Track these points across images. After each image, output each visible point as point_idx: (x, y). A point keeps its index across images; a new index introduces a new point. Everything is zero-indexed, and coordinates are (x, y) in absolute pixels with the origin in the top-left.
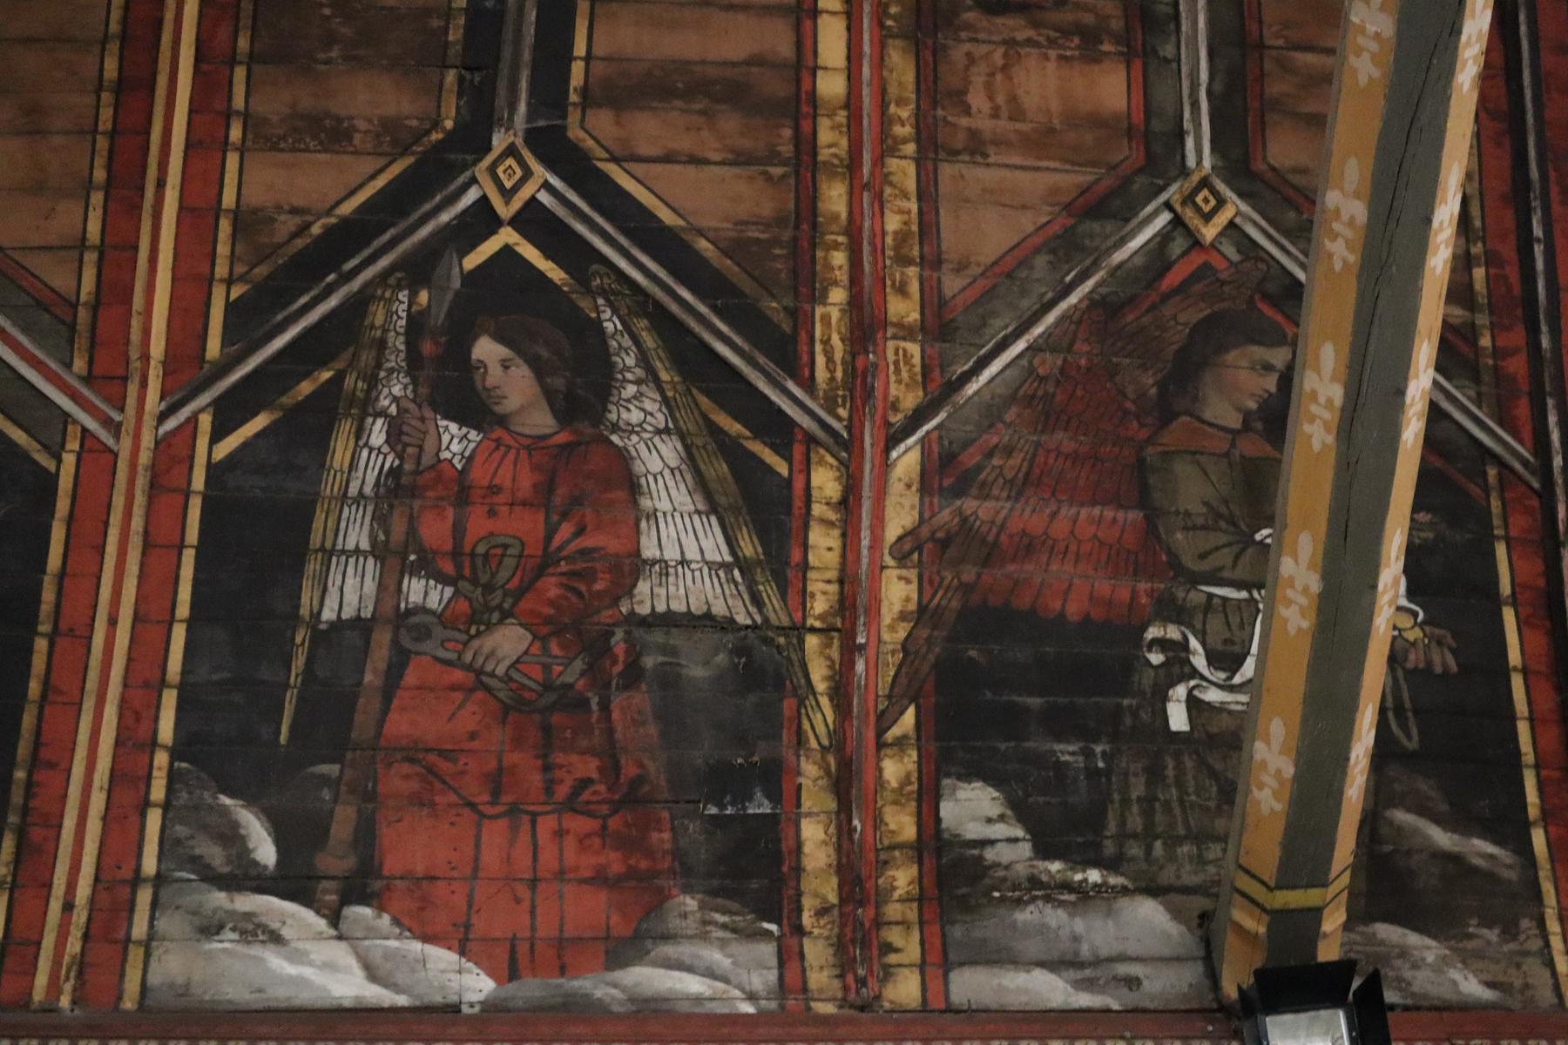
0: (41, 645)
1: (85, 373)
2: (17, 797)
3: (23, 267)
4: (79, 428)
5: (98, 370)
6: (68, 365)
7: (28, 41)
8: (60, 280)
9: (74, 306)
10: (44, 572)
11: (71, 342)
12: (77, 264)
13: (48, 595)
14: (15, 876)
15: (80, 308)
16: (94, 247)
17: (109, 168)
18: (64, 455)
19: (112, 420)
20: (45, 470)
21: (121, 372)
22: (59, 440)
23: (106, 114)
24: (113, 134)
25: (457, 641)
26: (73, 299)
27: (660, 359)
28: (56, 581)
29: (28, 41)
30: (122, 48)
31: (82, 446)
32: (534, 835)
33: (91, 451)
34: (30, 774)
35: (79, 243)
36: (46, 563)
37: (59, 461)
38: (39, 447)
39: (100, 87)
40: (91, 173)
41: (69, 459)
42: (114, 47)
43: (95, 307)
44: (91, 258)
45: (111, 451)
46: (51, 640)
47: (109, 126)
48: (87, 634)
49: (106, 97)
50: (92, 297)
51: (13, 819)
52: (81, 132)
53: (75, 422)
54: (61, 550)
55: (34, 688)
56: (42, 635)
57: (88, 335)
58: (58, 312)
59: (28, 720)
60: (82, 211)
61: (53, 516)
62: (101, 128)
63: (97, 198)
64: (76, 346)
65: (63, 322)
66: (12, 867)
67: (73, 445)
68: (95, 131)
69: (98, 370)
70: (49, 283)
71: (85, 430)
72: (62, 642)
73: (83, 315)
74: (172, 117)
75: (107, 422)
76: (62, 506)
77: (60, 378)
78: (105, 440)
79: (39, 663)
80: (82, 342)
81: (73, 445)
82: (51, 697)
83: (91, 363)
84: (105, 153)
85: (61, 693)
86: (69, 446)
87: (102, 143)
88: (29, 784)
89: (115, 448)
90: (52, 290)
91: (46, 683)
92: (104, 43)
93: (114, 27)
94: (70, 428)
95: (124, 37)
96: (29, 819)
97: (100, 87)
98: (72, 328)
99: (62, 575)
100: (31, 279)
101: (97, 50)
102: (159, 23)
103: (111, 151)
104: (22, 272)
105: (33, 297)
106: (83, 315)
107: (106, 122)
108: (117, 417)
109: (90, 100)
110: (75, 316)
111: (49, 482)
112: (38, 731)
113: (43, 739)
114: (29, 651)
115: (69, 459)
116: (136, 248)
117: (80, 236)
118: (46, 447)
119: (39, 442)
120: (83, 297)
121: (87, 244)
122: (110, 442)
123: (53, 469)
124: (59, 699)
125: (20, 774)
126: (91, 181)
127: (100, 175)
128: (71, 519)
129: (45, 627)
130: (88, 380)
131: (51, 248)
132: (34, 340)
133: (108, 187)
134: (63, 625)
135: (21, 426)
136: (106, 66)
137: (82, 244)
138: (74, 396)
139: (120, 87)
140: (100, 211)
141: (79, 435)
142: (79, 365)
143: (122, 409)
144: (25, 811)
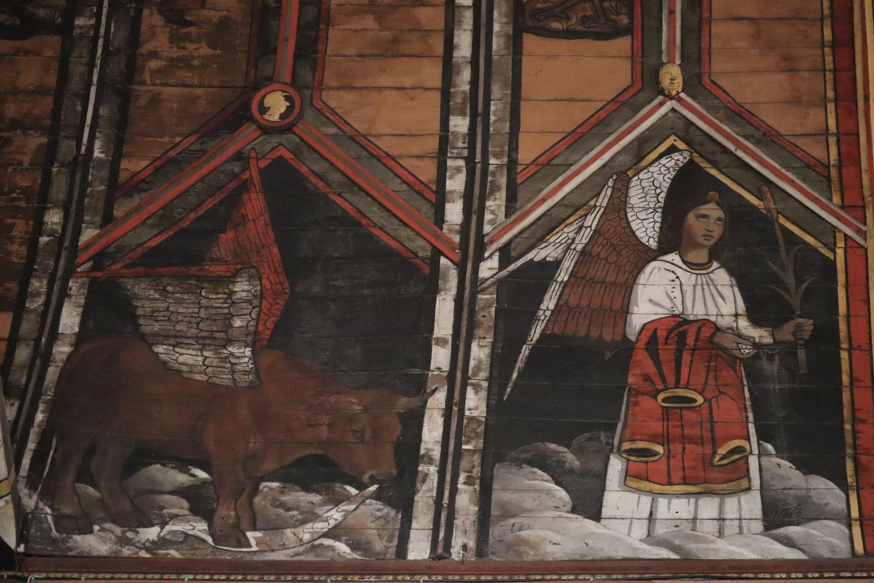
0: (844, 355)
1: (840, 204)
2: (849, 439)
3: (796, 146)
4: (843, 235)
5: (847, 202)
6: (831, 200)
7: (780, 19)
8: (817, 152)
9: (828, 167)
10: (838, 314)
11: (830, 187)
12: (825, 144)
13: (843, 327)
14: (857, 482)
15: (831, 168)
16: (833, 134)
17: (835, 89)
18: (837, 250)
19: (862, 230)
20: (828, 258)
21: (861, 204)
22: (833, 241)
23: (829, 59)
24: (835, 71)
25: (598, 239)
26: (827, 163)
27: (709, 85)
28: (845, 319)
29: (780, 19)
30: (832, 23)
31: (846, 244)
32: (148, 240)
33: (851, 247)
34: (853, 426)
35: (825, 132)
36: (838, 310)
37: (835, 253)
38: (822, 246)
39: (823, 45)
40: (826, 93)
41: (840, 252)
42: (828, 23)
43: (840, 167)
44: (832, 140)
45: (863, 247)
46: (850, 351)
47: (831, 66)
48: (869, 349)
49: (827, 50)
50: (837, 162)
51: (849, 451)
52: (818, 70)
53: (840, 231)
54: (845, 302)
55: (845, 379)
56: (844, 349)
57: (839, 183)
58: (818, 170)
59: (846, 397)
60: (824, 115)
61: (837, 283)
62: (827, 67)
63: (831, 107)
64: (833, 189)
65: (824, 176)
66: (854, 477)
67: (841, 244)
68: (825, 70)
69: (847, 202)
70: (812, 154)
71: (846, 236)
72: (856, 354)
73: (834, 172)
74: (867, 61)
75: (859, 231)
76: (841, 278)
77: (829, 207)
78: (859, 242)
79: (845, 365)
80: (835, 187)
81: (841, 244)
82: (855, 383)
83: (842, 198)
84: (832, 82)
85: (861, 381)
86: (838, 245)
87: (829, 76)
88: (854, 432)
89: (866, 246)
90: (813, 157)
91: (851, 375)
92: (822, 20)
93: (826, 11)
94: (837, 234)
95: (833, 17)
96: (858, 451)
97: (823, 45)
98: (829, 178)
99: (848, 316)
100: (801, 152)
101: (819, 24)
102: (851, 10)
103: (835, 80)
104: (795, 148)
105: (804, 162)
106: (834, 172)
107: (829, 65)
108: (864, 229)
109: (819, 52)
110: (829, 171)
111: (831, 265)
112: (853, 403)
113: (856, 407)
114: (838, 358)
115: (840, 252)
116: (858, 135)
117: (825, 128)
118: (826, 246)
119: (822, 243)
120: (832, 163)
121: (830, 132)
122: (862, 242)
123: (832, 257)
124: (861, 385)
125: (848, 427)
126: (826, 97)
127: (830, 94)
128: (847, 286)
129: (845, 345)
130: (843, 207)
131: (810, 135)
132: (811, 186)
133: (836, 100)
134: (854, 345)
135: (809, 233)
136: (825, 34)
137: (826, 132)
138: (839, 218)
139: (834, 45)
140: (834, 114)
141: (843, 238)
142: (837, 199)
143: (865, 224)
144: (855, 447)
